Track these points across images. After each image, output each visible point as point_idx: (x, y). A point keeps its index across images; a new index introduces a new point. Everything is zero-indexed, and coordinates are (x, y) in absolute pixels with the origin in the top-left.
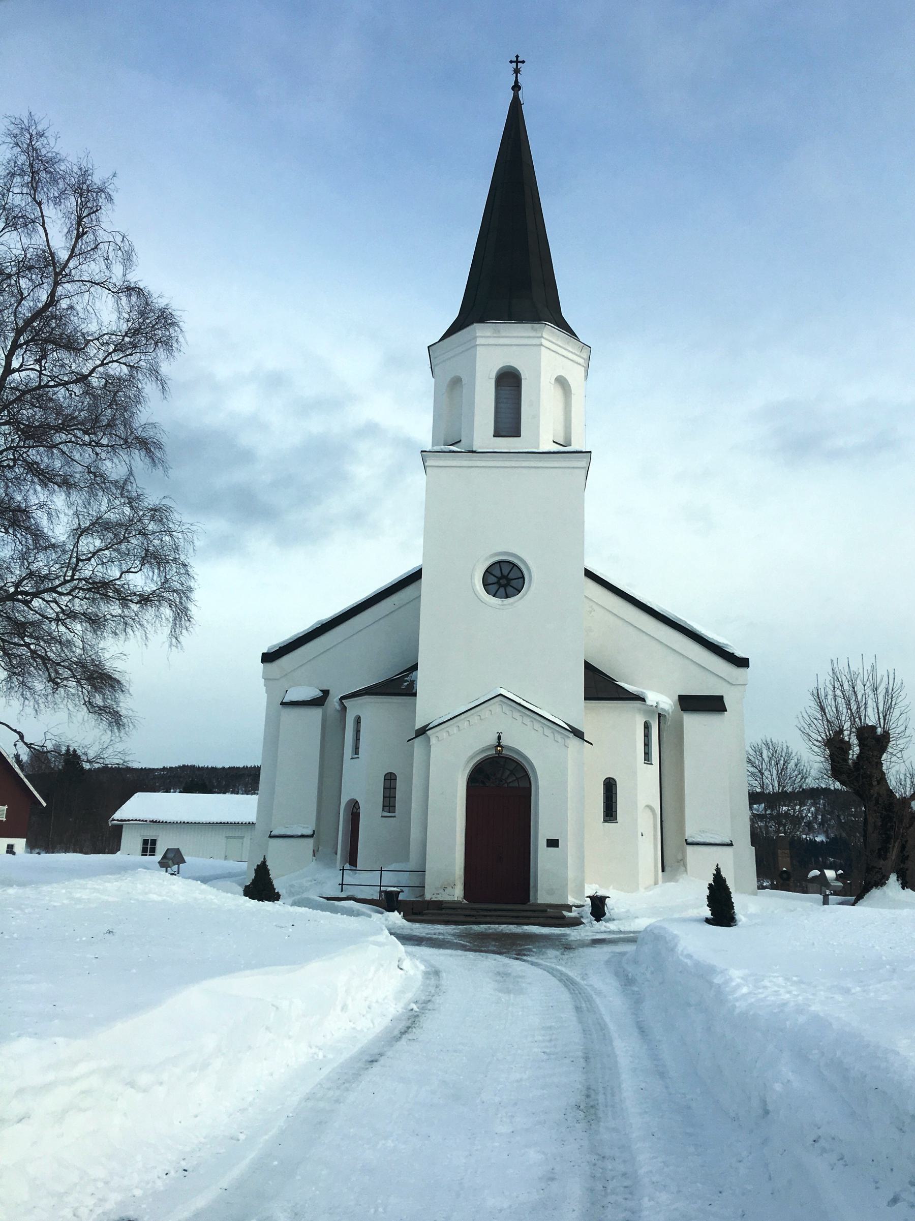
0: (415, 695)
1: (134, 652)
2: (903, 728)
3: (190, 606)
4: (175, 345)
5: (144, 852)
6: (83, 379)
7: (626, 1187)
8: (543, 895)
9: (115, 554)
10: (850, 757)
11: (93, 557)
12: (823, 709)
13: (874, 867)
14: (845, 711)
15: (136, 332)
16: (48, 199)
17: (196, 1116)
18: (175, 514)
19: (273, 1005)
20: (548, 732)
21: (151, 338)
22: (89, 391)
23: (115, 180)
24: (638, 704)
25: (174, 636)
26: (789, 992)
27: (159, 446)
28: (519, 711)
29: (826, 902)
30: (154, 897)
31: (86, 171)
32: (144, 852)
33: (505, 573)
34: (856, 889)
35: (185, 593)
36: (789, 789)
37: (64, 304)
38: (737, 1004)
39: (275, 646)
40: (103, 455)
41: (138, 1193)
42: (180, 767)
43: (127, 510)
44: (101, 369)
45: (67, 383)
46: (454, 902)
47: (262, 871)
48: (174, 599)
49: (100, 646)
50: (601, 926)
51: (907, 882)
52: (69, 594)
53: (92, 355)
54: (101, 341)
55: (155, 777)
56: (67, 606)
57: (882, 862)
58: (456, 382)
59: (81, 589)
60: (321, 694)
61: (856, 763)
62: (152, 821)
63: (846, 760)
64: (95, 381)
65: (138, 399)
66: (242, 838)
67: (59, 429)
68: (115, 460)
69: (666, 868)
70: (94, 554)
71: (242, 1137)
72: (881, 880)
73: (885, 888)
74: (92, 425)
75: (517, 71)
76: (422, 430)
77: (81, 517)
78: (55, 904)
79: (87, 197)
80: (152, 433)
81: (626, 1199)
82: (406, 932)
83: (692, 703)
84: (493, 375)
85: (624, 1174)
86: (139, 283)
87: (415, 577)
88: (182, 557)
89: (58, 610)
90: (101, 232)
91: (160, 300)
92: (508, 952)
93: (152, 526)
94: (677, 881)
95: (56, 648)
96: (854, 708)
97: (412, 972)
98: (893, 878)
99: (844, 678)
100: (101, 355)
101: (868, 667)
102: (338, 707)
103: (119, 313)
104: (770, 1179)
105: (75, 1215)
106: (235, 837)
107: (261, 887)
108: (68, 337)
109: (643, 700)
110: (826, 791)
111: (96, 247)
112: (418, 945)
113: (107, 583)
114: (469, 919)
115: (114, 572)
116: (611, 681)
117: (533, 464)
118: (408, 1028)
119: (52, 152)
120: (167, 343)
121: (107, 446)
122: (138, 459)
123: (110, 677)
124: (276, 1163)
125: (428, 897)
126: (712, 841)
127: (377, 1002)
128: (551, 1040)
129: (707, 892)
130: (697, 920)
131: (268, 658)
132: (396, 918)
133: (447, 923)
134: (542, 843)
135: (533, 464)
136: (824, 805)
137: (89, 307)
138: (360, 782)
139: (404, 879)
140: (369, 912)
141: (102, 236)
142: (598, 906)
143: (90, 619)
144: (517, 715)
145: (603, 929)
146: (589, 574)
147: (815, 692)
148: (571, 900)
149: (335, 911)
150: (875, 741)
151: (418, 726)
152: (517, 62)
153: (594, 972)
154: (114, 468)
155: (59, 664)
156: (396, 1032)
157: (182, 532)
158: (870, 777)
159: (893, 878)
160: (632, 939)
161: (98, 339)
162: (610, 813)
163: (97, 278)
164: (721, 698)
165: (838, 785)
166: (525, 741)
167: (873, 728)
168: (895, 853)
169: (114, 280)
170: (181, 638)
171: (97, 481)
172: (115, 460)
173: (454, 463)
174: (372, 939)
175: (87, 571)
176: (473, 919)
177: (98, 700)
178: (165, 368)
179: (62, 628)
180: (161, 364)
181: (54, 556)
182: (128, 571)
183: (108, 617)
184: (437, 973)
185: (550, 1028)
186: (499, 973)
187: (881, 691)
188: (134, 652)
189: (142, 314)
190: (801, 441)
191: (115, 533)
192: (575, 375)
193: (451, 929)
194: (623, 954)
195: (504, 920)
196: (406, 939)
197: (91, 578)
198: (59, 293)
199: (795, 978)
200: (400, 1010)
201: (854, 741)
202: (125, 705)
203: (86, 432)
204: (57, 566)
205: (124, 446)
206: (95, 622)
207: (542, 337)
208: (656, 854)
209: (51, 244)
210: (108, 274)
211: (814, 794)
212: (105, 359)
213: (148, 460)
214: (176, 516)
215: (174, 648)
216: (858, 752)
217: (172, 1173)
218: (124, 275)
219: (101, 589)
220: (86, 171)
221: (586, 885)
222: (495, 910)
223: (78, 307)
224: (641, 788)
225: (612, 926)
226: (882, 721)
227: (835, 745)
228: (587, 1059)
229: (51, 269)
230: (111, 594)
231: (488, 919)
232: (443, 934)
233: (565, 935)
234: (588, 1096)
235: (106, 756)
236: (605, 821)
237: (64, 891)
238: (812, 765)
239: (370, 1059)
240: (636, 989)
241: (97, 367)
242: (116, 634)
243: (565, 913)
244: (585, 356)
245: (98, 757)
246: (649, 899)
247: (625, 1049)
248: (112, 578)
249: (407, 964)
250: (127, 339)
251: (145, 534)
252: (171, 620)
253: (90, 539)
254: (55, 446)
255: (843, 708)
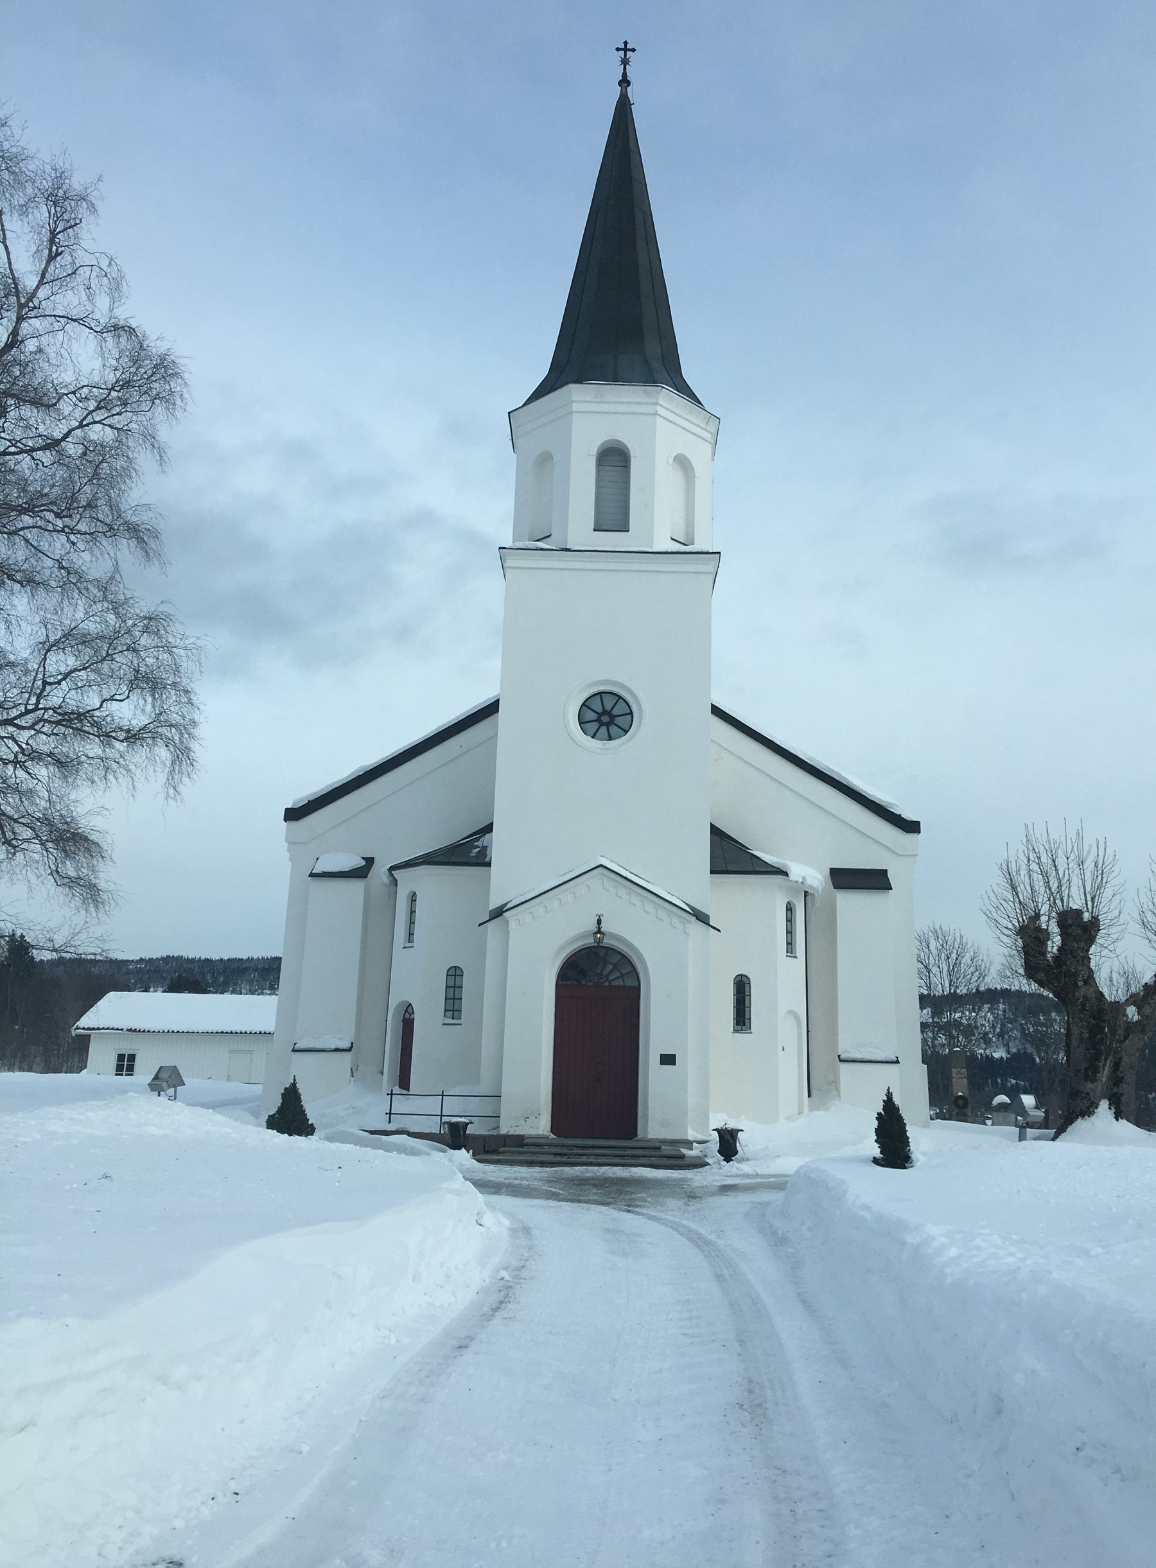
0: (489, 864)
1: (115, 804)
2: (1116, 913)
3: (194, 745)
4: (178, 402)
5: (119, 1070)
6: (53, 444)
7: (820, 1511)
8: (655, 1124)
9: (92, 676)
10: (1049, 949)
11: (64, 679)
12: (1014, 888)
13: (1079, 1092)
14: (1042, 890)
15: (127, 385)
16: (12, 207)
17: (242, 1422)
18: (177, 625)
19: (334, 1274)
20: (662, 914)
21: (146, 392)
22: (62, 459)
23: (101, 185)
24: (778, 879)
25: (172, 784)
26: (1012, 1255)
27: (156, 535)
28: (625, 887)
29: (1022, 1137)
30: (153, 1130)
31: (63, 172)
32: (119, 1070)
33: (608, 707)
34: (1060, 1119)
35: (186, 728)
36: (962, 990)
37: (31, 346)
38: (948, 1270)
39: (301, 799)
40: (81, 545)
41: (179, 1524)
42: (163, 959)
43: (111, 618)
44: (78, 432)
45: (33, 450)
46: (539, 1137)
47: (291, 1096)
48: (171, 737)
49: (72, 797)
50: (733, 1167)
51: (1121, 1112)
52: (31, 727)
53: (67, 413)
54: (78, 395)
55: (128, 972)
56: (27, 744)
57: (1089, 1085)
58: (545, 460)
59: (47, 721)
60: (363, 863)
61: (1056, 958)
62: (130, 1030)
63: (1043, 954)
64: (72, 448)
65: (126, 473)
66: (250, 1052)
67: (23, 511)
68: (95, 550)
69: (813, 1092)
70: (66, 676)
71: (305, 1449)
72: (1089, 1108)
73: (1093, 1118)
74: (67, 506)
75: (625, 62)
76: (497, 521)
77: (49, 626)
78: (26, 1140)
79: (63, 209)
80: (145, 518)
81: (822, 1527)
82: (478, 1176)
83: (847, 879)
84: (594, 451)
85: (815, 1494)
86: (130, 320)
87: (491, 709)
88: (185, 682)
89: (17, 749)
90: (80, 253)
91: (159, 343)
92: (615, 1203)
93: (145, 640)
94: (827, 1109)
95: (13, 799)
96: (1054, 886)
97: (494, 1229)
98: (1104, 1108)
99: (1042, 849)
100: (79, 414)
101: (1072, 834)
102: (386, 879)
103: (103, 358)
104: (1013, 1498)
105: (100, 1555)
106: (242, 1052)
107: (290, 1118)
108: (35, 389)
109: (786, 874)
110: (1005, 993)
111: (74, 273)
112: (495, 1193)
113: (83, 714)
114: (559, 1159)
115: (92, 700)
116: (742, 849)
117: (635, 567)
118: (501, 1303)
119: (17, 147)
120: (167, 399)
121: (85, 533)
122: (125, 550)
123: (86, 839)
124: (354, 1483)
125: (504, 1130)
126: (858, 1056)
127: (456, 1269)
128: (690, 1319)
129: (875, 1124)
130: (862, 1160)
131: (293, 815)
132: (463, 1156)
133: (531, 1164)
134: (655, 1060)
135: (635, 567)
136: (1004, 1011)
137: (62, 351)
138: (416, 981)
139: (474, 1106)
140: (426, 1150)
141: (82, 258)
142: (728, 1143)
143: (58, 761)
144: (622, 892)
145: (735, 1171)
146: (716, 711)
147: (1004, 866)
148: (692, 1135)
149: (389, 1148)
150: (1080, 930)
151: (494, 904)
152: (625, 50)
153: (730, 1225)
154: (92, 562)
155: (16, 821)
156: (486, 1309)
157: (186, 648)
158: (1076, 975)
159: (1104, 1104)
160: (778, 1184)
161: (74, 393)
162: (742, 1019)
163: (74, 314)
164: (884, 873)
165: (1034, 987)
166: (637, 930)
167: (1079, 913)
168: (1106, 1072)
169: (97, 316)
170: (181, 788)
171: (72, 579)
172: (95, 550)
173: (544, 564)
174: (445, 1185)
175: (54, 698)
176: (565, 1159)
177: (70, 869)
178: (163, 434)
179: (21, 773)
180: (158, 427)
181: (13, 678)
182: (112, 699)
183: (83, 758)
184: (527, 1230)
185: (687, 1302)
186: (608, 1231)
187: (1089, 865)
188: (115, 804)
189: (135, 361)
190: (976, 546)
191: (98, 650)
192: (698, 453)
193: (536, 1171)
194: (768, 1204)
195: (605, 1160)
196: (482, 1185)
197: (60, 707)
198: (25, 332)
199: (1014, 1237)
200: (487, 1280)
201: (1054, 928)
202: (106, 876)
203: (58, 515)
204: (15, 691)
205: (108, 534)
206: (65, 765)
207: (657, 404)
208: (800, 1074)
209: (14, 267)
210: (89, 307)
211: (992, 996)
212: (84, 419)
213: (139, 553)
214: (176, 628)
215: (170, 800)
216: (1059, 946)
217: (220, 1498)
218: (111, 310)
219: (74, 721)
220: (63, 172)
221: (711, 1115)
222: (593, 1147)
223: (48, 350)
224: (782, 989)
225: (746, 1168)
226: (1090, 903)
227: (1030, 935)
228: (741, 1342)
229: (13, 299)
230: (86, 729)
231: (584, 1159)
232: (526, 1179)
233: (684, 1180)
234: (751, 1392)
235: (78, 943)
236: (735, 1031)
237: (34, 1122)
238: (997, 960)
239: (458, 1344)
240: (791, 1250)
241: (74, 429)
242: (93, 782)
243: (684, 1151)
244: (713, 429)
245: (68, 944)
246: (803, 1136)
247: (791, 1331)
248: (89, 708)
249: (488, 1219)
250: (114, 394)
251: (134, 650)
252: (168, 763)
253: (61, 656)
254: (15, 533)
255: (1040, 887)
